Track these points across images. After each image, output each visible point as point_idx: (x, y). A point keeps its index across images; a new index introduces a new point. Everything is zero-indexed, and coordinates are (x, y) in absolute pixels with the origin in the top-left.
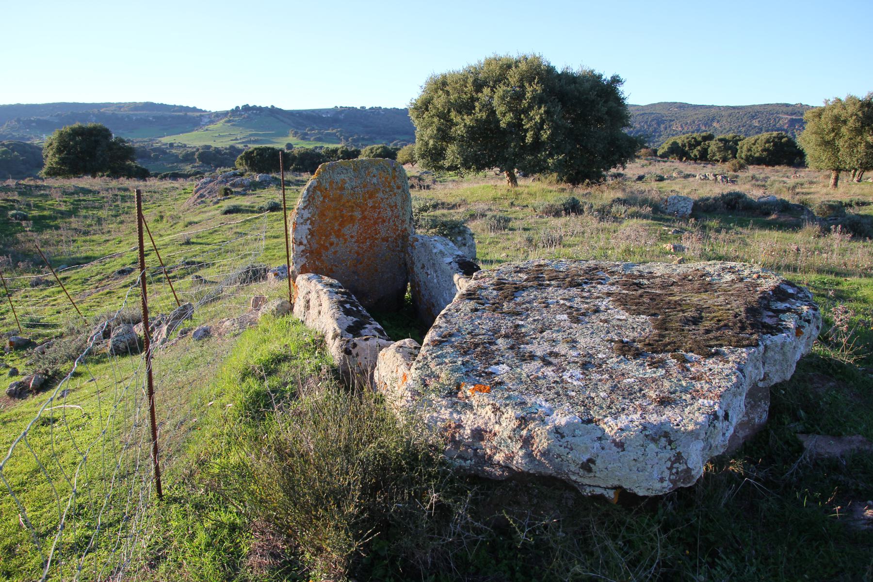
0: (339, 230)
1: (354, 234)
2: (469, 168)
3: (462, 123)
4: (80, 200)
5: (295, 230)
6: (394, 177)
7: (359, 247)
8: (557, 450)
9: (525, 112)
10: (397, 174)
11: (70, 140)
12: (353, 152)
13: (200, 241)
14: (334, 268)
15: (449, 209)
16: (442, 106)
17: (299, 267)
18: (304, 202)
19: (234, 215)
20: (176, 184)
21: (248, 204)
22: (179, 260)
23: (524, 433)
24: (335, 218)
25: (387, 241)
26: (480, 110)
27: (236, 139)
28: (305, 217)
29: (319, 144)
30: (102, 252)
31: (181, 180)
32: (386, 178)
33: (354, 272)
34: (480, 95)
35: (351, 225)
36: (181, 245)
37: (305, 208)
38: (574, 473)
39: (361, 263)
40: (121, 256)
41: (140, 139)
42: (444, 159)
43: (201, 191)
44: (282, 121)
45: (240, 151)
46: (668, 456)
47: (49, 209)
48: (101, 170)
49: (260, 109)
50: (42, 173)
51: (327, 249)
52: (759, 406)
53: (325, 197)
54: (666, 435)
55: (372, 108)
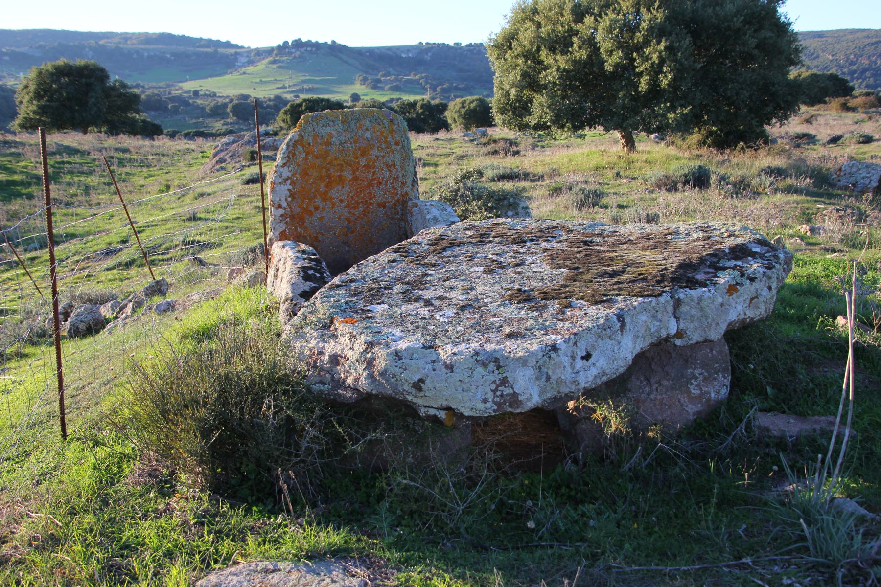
0: (326, 193)
1: (344, 197)
2: (562, 127)
3: (555, 65)
4: (63, 163)
5: (273, 190)
6: (392, 131)
7: (350, 213)
8: (392, 370)
9: (639, 48)
10: (395, 127)
11: (53, 81)
12: (437, 106)
15: (532, 181)
16: (531, 43)
17: (277, 234)
20: (192, 145)
22: (178, 240)
23: (368, 355)
24: (321, 178)
25: (384, 207)
26: (580, 48)
27: (284, 87)
28: (285, 175)
29: (395, 96)
30: (87, 229)
31: (200, 141)
32: (382, 132)
33: (344, 243)
34: (580, 26)
37: (284, 165)
38: (409, 393)
39: (352, 232)
40: (107, 232)
41: (154, 84)
42: (530, 115)
43: (221, 155)
44: (346, 62)
45: (286, 102)
46: (493, 379)
47: (21, 172)
48: (94, 123)
49: (317, 45)
50: (15, 124)
51: (311, 214)
52: (715, 379)
53: (308, 153)
54: (496, 361)
55: (470, 45)
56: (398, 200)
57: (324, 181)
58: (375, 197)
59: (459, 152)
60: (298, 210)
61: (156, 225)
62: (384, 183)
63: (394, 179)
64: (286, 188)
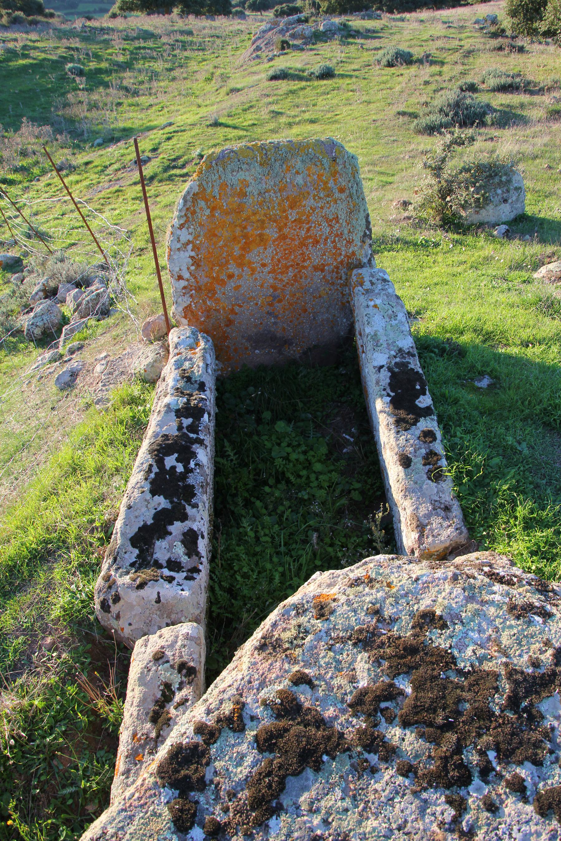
0: (242, 256)
1: (268, 261)
4: (140, 48)
6: (334, 174)
7: (276, 279)
13: (230, 122)
14: (237, 309)
17: (180, 309)
18: (180, 217)
19: (280, 81)
21: (299, 66)
25: (322, 270)
28: (184, 239)
33: (268, 313)
35: (261, 249)
36: (208, 126)
37: (181, 227)
39: (280, 301)
42: (541, 20)
43: (258, 43)
51: (223, 283)
53: (213, 209)
56: (342, 262)
57: (239, 242)
58: (309, 258)
59: (467, 44)
60: (206, 280)
61: (184, 131)
62: (322, 241)
63: (337, 235)
64: (187, 254)
